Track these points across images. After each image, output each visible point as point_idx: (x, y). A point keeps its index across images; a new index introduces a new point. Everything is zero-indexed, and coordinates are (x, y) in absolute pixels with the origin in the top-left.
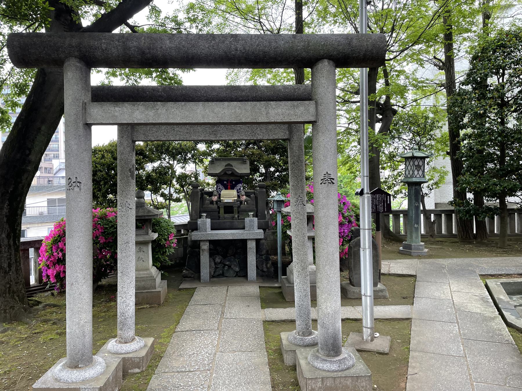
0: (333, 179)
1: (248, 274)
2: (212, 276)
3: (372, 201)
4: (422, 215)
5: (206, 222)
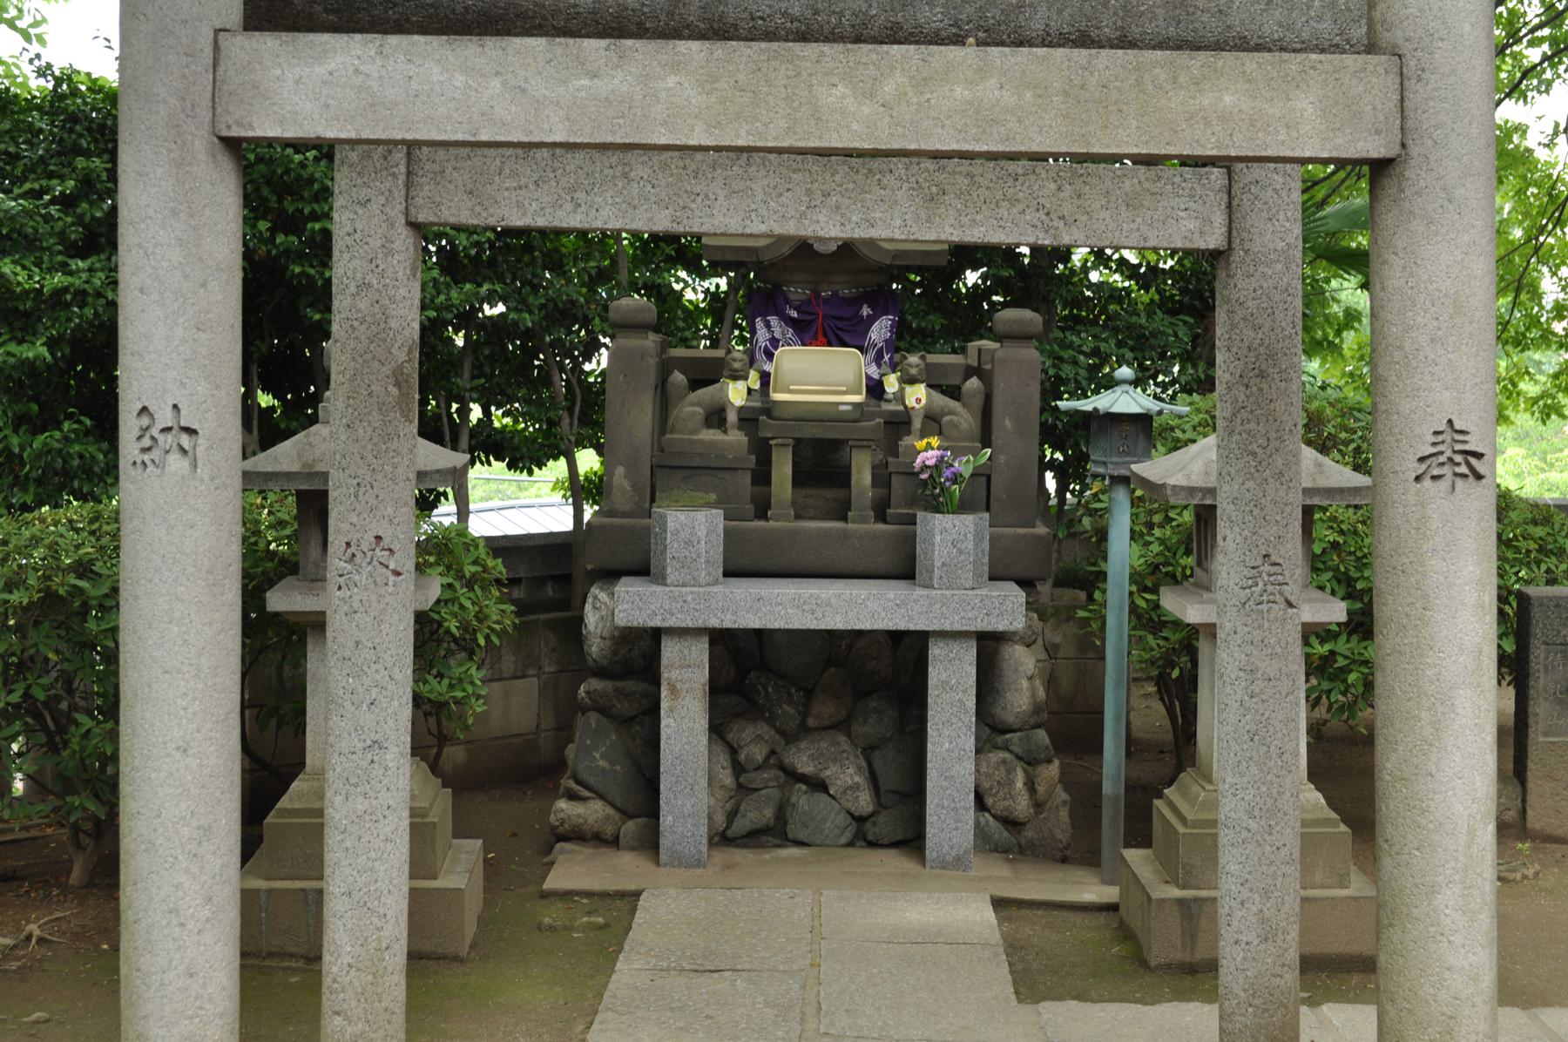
0: (1479, 456)
2: (722, 839)
5: (692, 529)
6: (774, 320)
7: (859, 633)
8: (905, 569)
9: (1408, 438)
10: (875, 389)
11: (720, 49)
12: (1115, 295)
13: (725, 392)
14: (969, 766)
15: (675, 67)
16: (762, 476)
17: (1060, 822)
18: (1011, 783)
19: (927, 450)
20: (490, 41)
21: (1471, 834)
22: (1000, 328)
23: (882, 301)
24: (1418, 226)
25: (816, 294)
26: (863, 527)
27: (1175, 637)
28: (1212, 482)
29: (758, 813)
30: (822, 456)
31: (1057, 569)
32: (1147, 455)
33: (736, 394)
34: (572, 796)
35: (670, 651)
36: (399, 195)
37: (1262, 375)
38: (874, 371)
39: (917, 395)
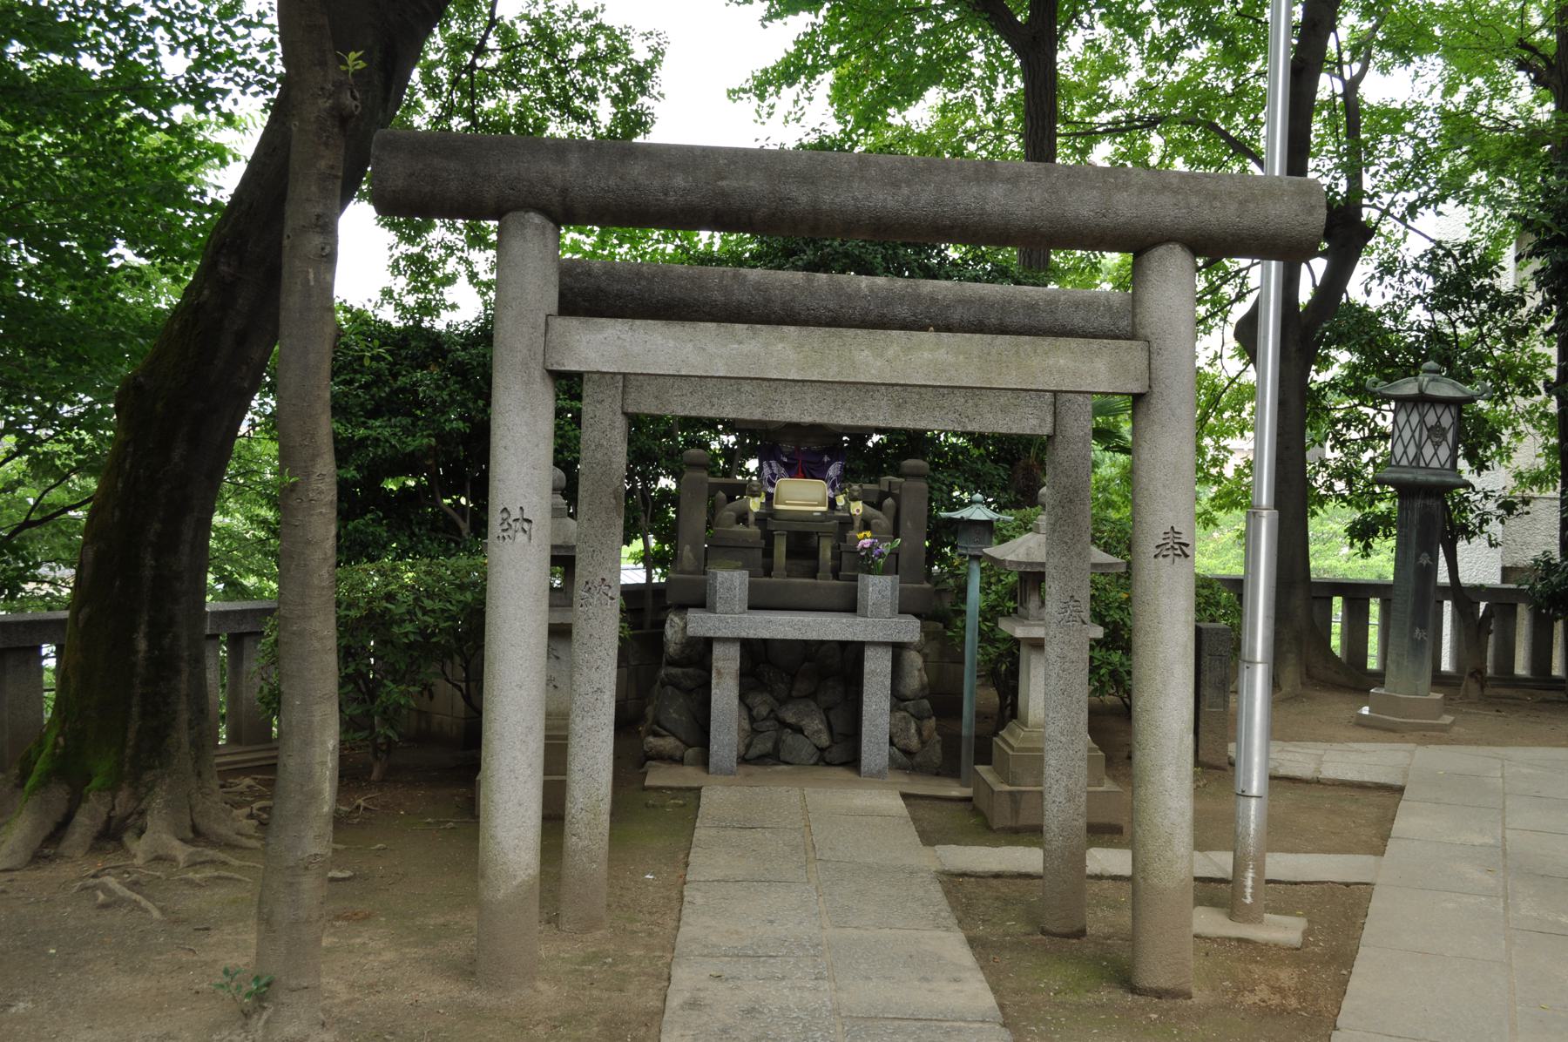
1: (864, 756)
2: (743, 760)
3: (347, 654)
4: (1448, 606)
5: (731, 582)
6: (773, 463)
7: (822, 642)
8: (850, 606)
9: (1150, 539)
10: (832, 503)
11: (805, 331)
12: (964, 451)
13: (747, 502)
14: (887, 718)
15: (782, 339)
16: (768, 552)
17: (936, 754)
18: (908, 730)
19: (865, 540)
20: (687, 324)
21: (1181, 739)
22: (905, 470)
23: (835, 451)
24: (1156, 428)
25: (798, 448)
26: (825, 582)
27: (1003, 647)
28: (1043, 559)
29: (763, 745)
30: (802, 540)
31: (936, 610)
32: (990, 544)
33: (755, 504)
34: (656, 735)
35: (718, 651)
36: (619, 398)
37: (1071, 501)
38: (829, 493)
39: (857, 508)
